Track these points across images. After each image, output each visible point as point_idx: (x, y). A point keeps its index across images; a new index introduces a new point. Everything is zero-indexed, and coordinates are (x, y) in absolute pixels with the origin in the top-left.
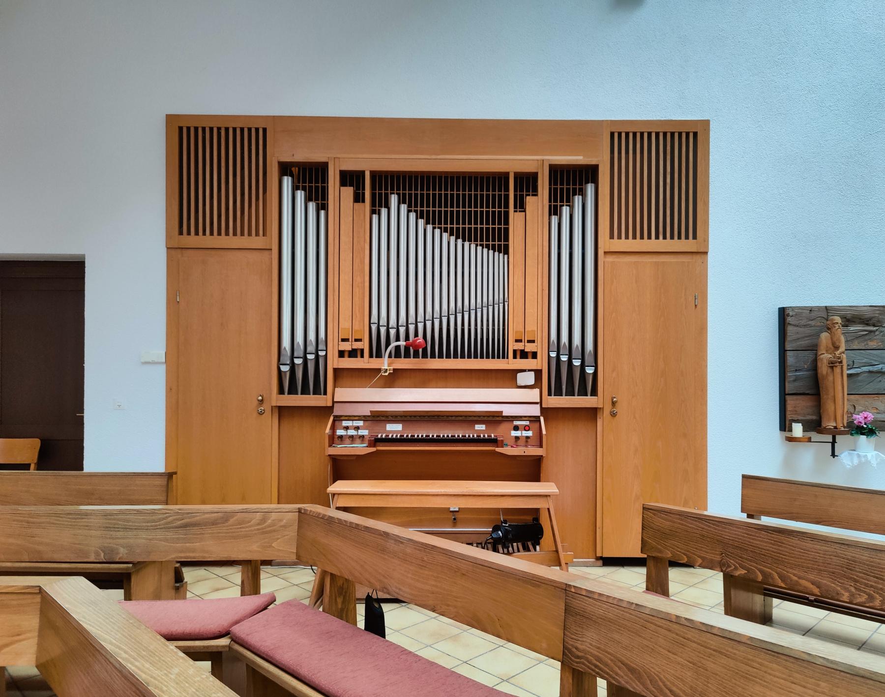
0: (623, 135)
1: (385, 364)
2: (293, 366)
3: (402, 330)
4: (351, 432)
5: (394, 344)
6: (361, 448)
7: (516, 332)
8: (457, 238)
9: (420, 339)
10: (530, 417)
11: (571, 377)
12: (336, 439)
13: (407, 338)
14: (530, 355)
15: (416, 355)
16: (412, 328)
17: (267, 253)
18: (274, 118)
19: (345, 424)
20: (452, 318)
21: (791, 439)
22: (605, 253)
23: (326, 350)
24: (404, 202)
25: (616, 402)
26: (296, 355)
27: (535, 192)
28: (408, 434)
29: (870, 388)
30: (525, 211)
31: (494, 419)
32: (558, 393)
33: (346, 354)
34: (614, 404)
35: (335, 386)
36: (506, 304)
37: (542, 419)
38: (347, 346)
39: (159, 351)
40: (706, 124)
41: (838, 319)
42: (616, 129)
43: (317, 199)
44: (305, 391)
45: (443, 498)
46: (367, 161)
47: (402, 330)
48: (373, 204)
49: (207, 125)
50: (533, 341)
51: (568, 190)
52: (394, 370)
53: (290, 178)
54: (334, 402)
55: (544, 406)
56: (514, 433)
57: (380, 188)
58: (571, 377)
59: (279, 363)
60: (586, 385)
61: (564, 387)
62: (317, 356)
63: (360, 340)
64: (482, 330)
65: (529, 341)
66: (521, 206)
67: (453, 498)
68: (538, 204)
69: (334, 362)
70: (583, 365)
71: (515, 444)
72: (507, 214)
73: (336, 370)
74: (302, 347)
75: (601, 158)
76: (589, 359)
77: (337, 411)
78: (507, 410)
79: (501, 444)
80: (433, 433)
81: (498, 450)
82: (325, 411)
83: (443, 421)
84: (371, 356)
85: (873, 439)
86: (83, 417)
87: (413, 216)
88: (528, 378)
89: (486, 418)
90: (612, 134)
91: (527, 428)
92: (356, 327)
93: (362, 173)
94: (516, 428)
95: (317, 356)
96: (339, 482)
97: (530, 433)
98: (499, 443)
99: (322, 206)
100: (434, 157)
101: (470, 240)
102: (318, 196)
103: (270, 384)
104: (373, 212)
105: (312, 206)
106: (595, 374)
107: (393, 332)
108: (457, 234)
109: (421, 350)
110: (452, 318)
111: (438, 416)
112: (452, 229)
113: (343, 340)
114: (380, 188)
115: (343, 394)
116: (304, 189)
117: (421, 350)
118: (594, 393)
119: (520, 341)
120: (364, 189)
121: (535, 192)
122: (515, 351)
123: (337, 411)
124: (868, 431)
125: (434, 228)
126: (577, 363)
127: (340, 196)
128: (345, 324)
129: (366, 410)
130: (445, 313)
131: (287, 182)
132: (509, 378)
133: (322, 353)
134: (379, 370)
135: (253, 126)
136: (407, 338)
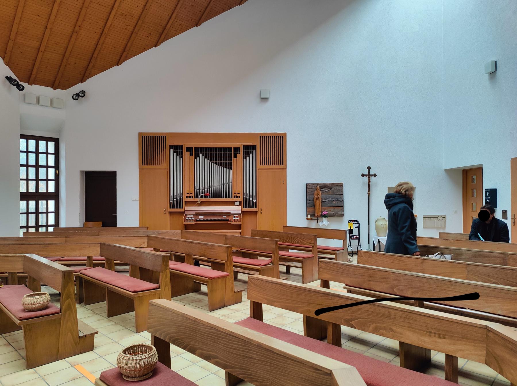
1: (199, 200)
2: (174, 201)
4: (190, 218)
6: (193, 223)
9: (208, 193)
11: (249, 203)
15: (207, 197)
21: (307, 219)
29: (329, 205)
31: (228, 214)
32: (246, 207)
38: (188, 195)
39: (137, 197)
40: (285, 134)
41: (319, 187)
42: (261, 135)
44: (177, 207)
46: (193, 145)
48: (195, 156)
49: (150, 135)
57: (197, 152)
58: (249, 203)
59: (170, 200)
60: (254, 205)
66: (235, 156)
68: (240, 156)
69: (185, 199)
70: (253, 200)
71: (234, 220)
75: (257, 143)
76: (254, 198)
78: (232, 212)
80: (215, 218)
82: (183, 213)
85: (327, 218)
86: (116, 216)
87: (206, 159)
94: (234, 217)
99: (181, 157)
104: (195, 158)
105: (178, 157)
108: (219, 164)
114: (197, 152)
115: (187, 208)
118: (256, 207)
124: (325, 216)
127: (186, 154)
128: (188, 189)
129: (194, 212)
131: (172, 151)
132: (232, 203)
135: (162, 135)
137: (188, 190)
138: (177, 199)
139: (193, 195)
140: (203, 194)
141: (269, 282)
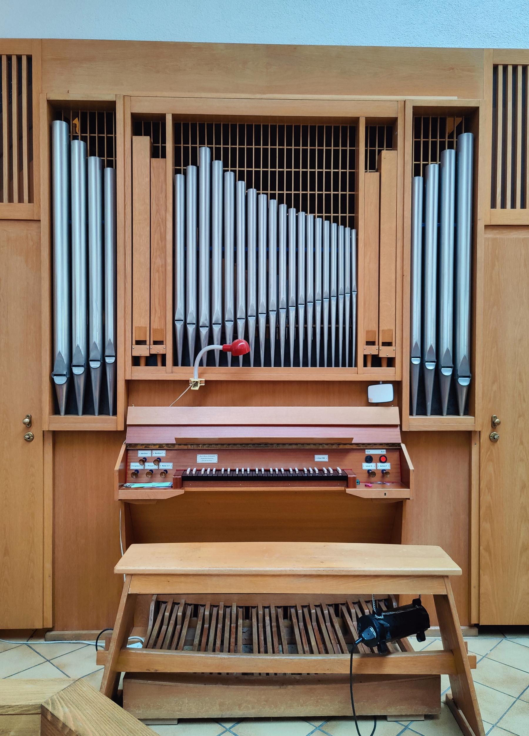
0: (510, 69)
1: (195, 375)
3: (217, 329)
4: (150, 466)
5: (205, 349)
6: (161, 489)
10: (387, 444)
12: (129, 476)
13: (223, 340)
14: (384, 362)
15: (235, 363)
16: (229, 326)
17: (34, 225)
18: (42, 41)
19: (142, 454)
22: (487, 227)
23: (116, 356)
24: (218, 158)
25: (499, 423)
26: (74, 362)
27: (392, 145)
28: (226, 468)
30: (379, 170)
31: (339, 448)
32: (422, 411)
33: (143, 361)
34: (494, 425)
35: (128, 404)
36: (354, 294)
37: (403, 446)
38: (143, 351)
43: (101, 155)
44: (88, 410)
45: (288, 579)
47: (217, 329)
48: (177, 162)
50: (389, 344)
51: (434, 144)
52: (206, 382)
53: (64, 124)
54: (126, 426)
55: (403, 430)
56: (366, 466)
57: (188, 137)
58: (440, 389)
61: (429, 404)
62: (104, 365)
63: (160, 343)
64: (314, 329)
65: (385, 344)
66: (373, 164)
67: (303, 580)
68: (397, 160)
69: (126, 372)
72: (354, 177)
73: (129, 383)
74: (99, 347)
77: (132, 437)
78: (359, 436)
79: (354, 483)
81: (349, 491)
83: (272, 450)
84: (175, 364)
87: (230, 176)
88: (383, 393)
89: (326, 447)
90: (495, 68)
91: (383, 459)
92: (155, 326)
93: (162, 117)
94: (369, 459)
95: (104, 365)
96: (134, 548)
97: (387, 466)
98: (351, 483)
100: (258, 96)
101: (305, 210)
102: (103, 148)
103: (40, 401)
104: (177, 172)
106: (471, 388)
107: (204, 332)
109: (241, 357)
111: (266, 444)
113: (138, 343)
115: (138, 414)
116: (84, 139)
117: (241, 357)
118: (469, 410)
119: (373, 343)
120: (164, 141)
121: (392, 145)
122: (365, 356)
123: (132, 437)
126: (447, 372)
127: (132, 148)
128: (141, 321)
129: (169, 436)
130: (252, 310)
131: (60, 127)
132: (358, 392)
133: (110, 360)
134: (187, 382)
136: (223, 340)
137: (141, 321)
138: (88, 370)
139: (167, 349)
140: (217, 347)
141: (296, 493)
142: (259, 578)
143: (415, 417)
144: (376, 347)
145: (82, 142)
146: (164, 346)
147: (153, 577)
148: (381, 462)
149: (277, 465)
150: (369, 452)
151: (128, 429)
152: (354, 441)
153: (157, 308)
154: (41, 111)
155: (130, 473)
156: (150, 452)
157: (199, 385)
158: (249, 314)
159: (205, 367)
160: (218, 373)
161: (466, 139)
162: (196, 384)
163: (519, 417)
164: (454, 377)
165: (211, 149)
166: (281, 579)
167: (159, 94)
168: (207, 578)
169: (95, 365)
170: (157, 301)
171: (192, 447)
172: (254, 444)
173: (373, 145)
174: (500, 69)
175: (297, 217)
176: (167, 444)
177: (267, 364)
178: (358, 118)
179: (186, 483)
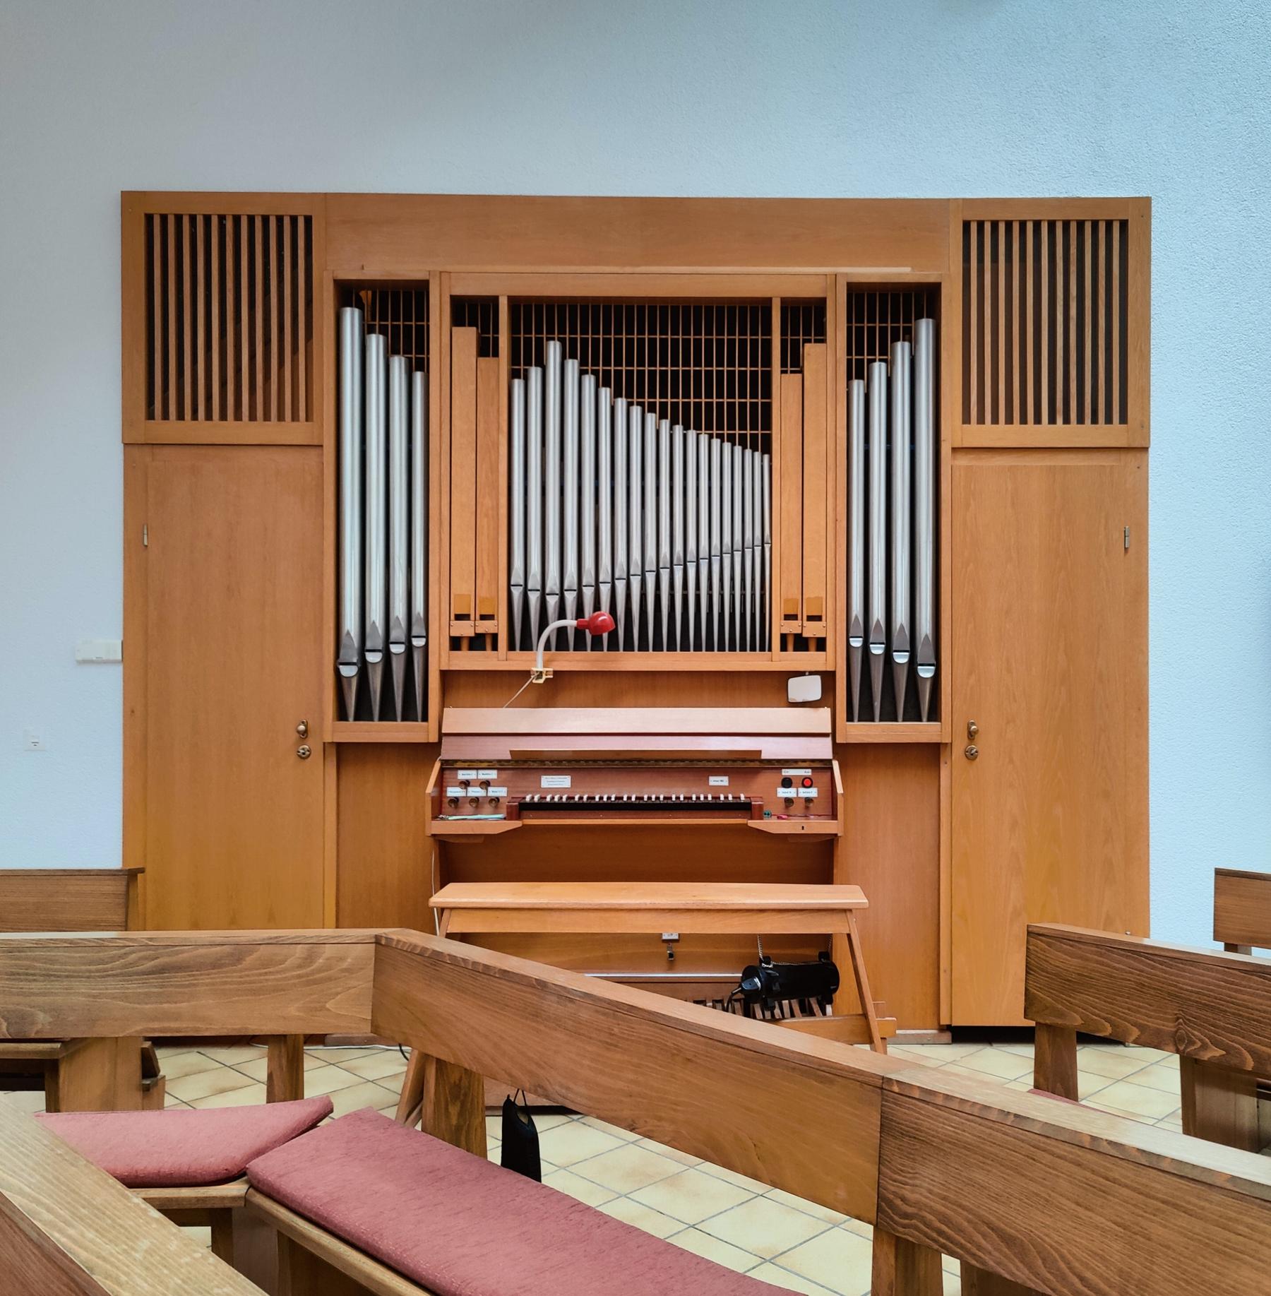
1: (538, 662)
3: (570, 597)
4: (475, 792)
5: (554, 625)
6: (493, 823)
7: (787, 601)
8: (674, 422)
10: (813, 761)
14: (812, 645)
15: (597, 646)
16: (588, 593)
19: (463, 775)
20: (665, 575)
22: (954, 450)
23: (427, 637)
24: (573, 356)
25: (976, 732)
26: (369, 645)
27: (820, 335)
31: (745, 765)
32: (867, 715)
33: (465, 644)
34: (971, 735)
35: (443, 705)
36: (767, 547)
37: (836, 765)
38: (465, 629)
43: (407, 351)
44: (387, 714)
47: (570, 597)
48: (514, 359)
50: (818, 618)
52: (555, 672)
53: (357, 311)
54: (441, 735)
55: (838, 741)
56: (783, 793)
57: (526, 328)
58: (889, 681)
61: (877, 704)
62: (410, 649)
64: (710, 597)
65: (810, 618)
66: (794, 362)
67: (668, 915)
68: (825, 358)
69: (442, 659)
72: (767, 377)
73: (444, 675)
74: (403, 623)
77: (448, 752)
78: (771, 749)
81: (753, 823)
83: (648, 770)
84: (511, 647)
87: (589, 381)
88: (809, 688)
89: (729, 765)
90: (966, 225)
91: (807, 782)
92: (483, 592)
93: (494, 300)
94: (787, 783)
95: (410, 649)
97: (812, 793)
100: (628, 269)
101: (698, 427)
102: (410, 344)
103: (321, 700)
104: (514, 374)
106: (936, 679)
107: (552, 601)
109: (605, 636)
110: (665, 575)
111: (639, 760)
112: (663, 405)
113: (459, 617)
115: (459, 719)
116: (383, 331)
118: (935, 715)
119: (794, 617)
120: (496, 331)
121: (820, 335)
122: (784, 637)
123: (448, 752)
125: (630, 404)
126: (901, 658)
127: (451, 344)
128: (462, 586)
129: (502, 750)
130: (620, 571)
131: (351, 318)
132: (772, 687)
134: (526, 674)
138: (387, 655)
139: (499, 626)
142: (613, 914)
143: (856, 723)
144: (799, 622)
145: (381, 337)
146: (495, 622)
147: (478, 912)
148: (804, 786)
149: (655, 791)
150: (787, 773)
151: (444, 739)
152: (764, 756)
153: (486, 569)
154: (325, 294)
155: (446, 801)
156: (474, 772)
157: (544, 677)
158: (617, 576)
159: (553, 651)
160: (572, 661)
161: (924, 328)
162: (540, 675)
163: (1008, 722)
164: (913, 664)
165: (562, 341)
166: (640, 915)
167: (489, 268)
168: (546, 913)
169: (397, 649)
170: (485, 557)
171: (536, 766)
172: (622, 761)
173: (795, 332)
174: (974, 227)
175: (685, 436)
176: (499, 761)
177: (643, 647)
178: (770, 299)
179: (525, 813)
